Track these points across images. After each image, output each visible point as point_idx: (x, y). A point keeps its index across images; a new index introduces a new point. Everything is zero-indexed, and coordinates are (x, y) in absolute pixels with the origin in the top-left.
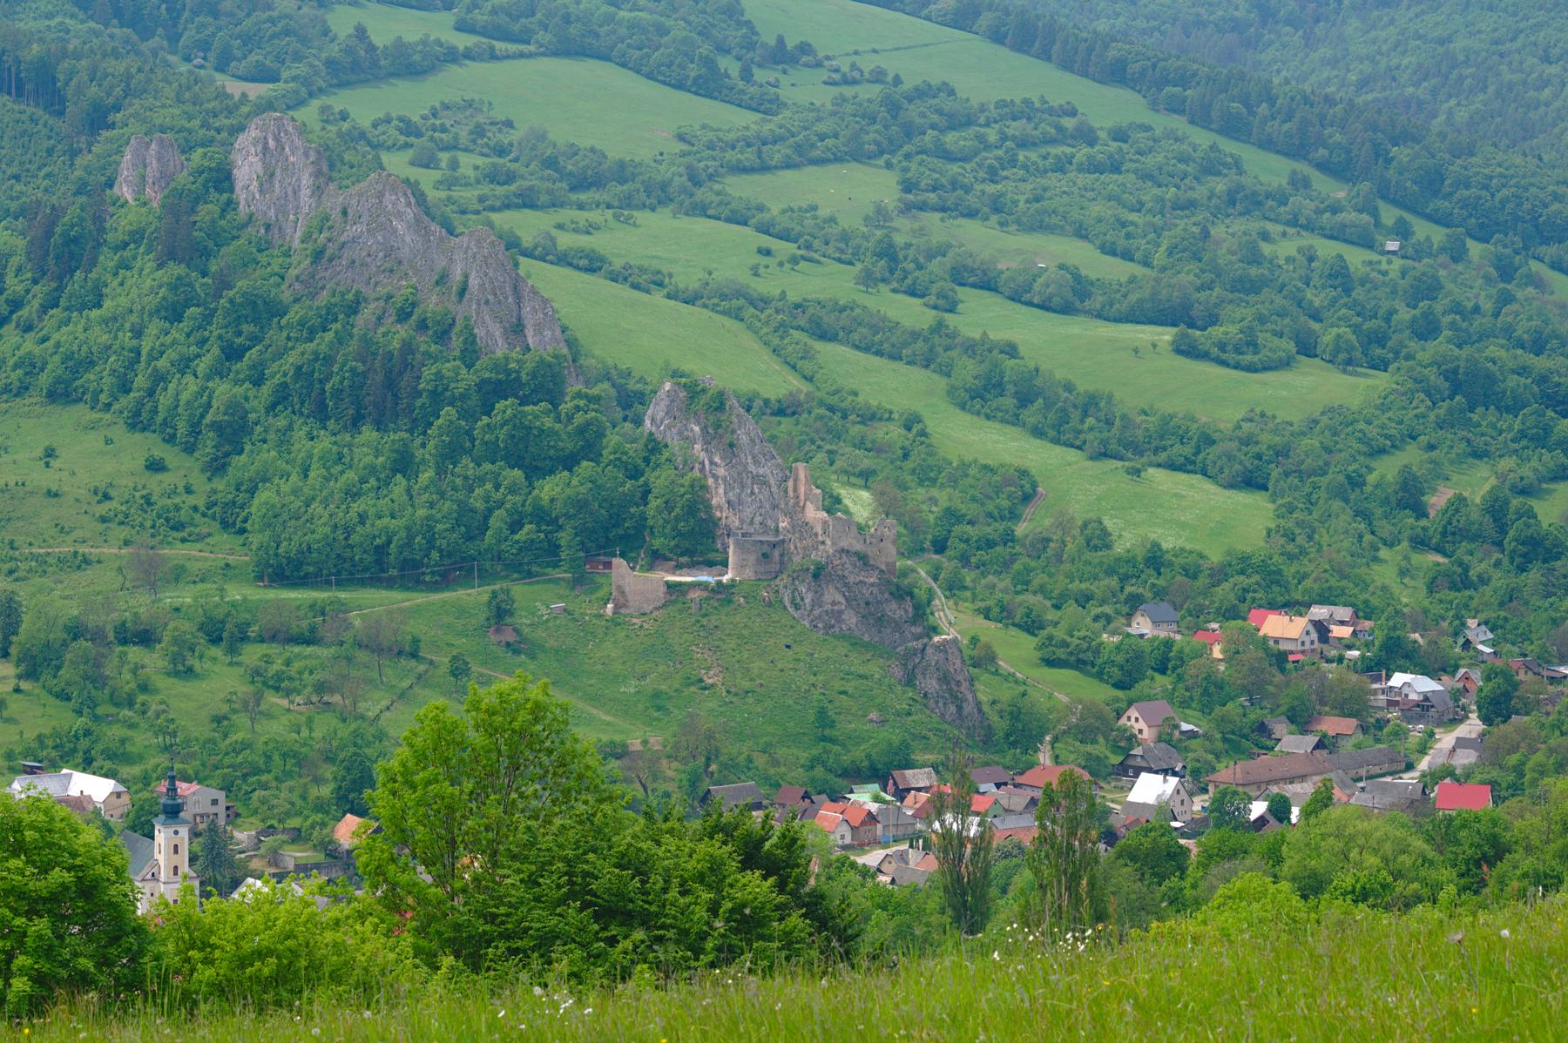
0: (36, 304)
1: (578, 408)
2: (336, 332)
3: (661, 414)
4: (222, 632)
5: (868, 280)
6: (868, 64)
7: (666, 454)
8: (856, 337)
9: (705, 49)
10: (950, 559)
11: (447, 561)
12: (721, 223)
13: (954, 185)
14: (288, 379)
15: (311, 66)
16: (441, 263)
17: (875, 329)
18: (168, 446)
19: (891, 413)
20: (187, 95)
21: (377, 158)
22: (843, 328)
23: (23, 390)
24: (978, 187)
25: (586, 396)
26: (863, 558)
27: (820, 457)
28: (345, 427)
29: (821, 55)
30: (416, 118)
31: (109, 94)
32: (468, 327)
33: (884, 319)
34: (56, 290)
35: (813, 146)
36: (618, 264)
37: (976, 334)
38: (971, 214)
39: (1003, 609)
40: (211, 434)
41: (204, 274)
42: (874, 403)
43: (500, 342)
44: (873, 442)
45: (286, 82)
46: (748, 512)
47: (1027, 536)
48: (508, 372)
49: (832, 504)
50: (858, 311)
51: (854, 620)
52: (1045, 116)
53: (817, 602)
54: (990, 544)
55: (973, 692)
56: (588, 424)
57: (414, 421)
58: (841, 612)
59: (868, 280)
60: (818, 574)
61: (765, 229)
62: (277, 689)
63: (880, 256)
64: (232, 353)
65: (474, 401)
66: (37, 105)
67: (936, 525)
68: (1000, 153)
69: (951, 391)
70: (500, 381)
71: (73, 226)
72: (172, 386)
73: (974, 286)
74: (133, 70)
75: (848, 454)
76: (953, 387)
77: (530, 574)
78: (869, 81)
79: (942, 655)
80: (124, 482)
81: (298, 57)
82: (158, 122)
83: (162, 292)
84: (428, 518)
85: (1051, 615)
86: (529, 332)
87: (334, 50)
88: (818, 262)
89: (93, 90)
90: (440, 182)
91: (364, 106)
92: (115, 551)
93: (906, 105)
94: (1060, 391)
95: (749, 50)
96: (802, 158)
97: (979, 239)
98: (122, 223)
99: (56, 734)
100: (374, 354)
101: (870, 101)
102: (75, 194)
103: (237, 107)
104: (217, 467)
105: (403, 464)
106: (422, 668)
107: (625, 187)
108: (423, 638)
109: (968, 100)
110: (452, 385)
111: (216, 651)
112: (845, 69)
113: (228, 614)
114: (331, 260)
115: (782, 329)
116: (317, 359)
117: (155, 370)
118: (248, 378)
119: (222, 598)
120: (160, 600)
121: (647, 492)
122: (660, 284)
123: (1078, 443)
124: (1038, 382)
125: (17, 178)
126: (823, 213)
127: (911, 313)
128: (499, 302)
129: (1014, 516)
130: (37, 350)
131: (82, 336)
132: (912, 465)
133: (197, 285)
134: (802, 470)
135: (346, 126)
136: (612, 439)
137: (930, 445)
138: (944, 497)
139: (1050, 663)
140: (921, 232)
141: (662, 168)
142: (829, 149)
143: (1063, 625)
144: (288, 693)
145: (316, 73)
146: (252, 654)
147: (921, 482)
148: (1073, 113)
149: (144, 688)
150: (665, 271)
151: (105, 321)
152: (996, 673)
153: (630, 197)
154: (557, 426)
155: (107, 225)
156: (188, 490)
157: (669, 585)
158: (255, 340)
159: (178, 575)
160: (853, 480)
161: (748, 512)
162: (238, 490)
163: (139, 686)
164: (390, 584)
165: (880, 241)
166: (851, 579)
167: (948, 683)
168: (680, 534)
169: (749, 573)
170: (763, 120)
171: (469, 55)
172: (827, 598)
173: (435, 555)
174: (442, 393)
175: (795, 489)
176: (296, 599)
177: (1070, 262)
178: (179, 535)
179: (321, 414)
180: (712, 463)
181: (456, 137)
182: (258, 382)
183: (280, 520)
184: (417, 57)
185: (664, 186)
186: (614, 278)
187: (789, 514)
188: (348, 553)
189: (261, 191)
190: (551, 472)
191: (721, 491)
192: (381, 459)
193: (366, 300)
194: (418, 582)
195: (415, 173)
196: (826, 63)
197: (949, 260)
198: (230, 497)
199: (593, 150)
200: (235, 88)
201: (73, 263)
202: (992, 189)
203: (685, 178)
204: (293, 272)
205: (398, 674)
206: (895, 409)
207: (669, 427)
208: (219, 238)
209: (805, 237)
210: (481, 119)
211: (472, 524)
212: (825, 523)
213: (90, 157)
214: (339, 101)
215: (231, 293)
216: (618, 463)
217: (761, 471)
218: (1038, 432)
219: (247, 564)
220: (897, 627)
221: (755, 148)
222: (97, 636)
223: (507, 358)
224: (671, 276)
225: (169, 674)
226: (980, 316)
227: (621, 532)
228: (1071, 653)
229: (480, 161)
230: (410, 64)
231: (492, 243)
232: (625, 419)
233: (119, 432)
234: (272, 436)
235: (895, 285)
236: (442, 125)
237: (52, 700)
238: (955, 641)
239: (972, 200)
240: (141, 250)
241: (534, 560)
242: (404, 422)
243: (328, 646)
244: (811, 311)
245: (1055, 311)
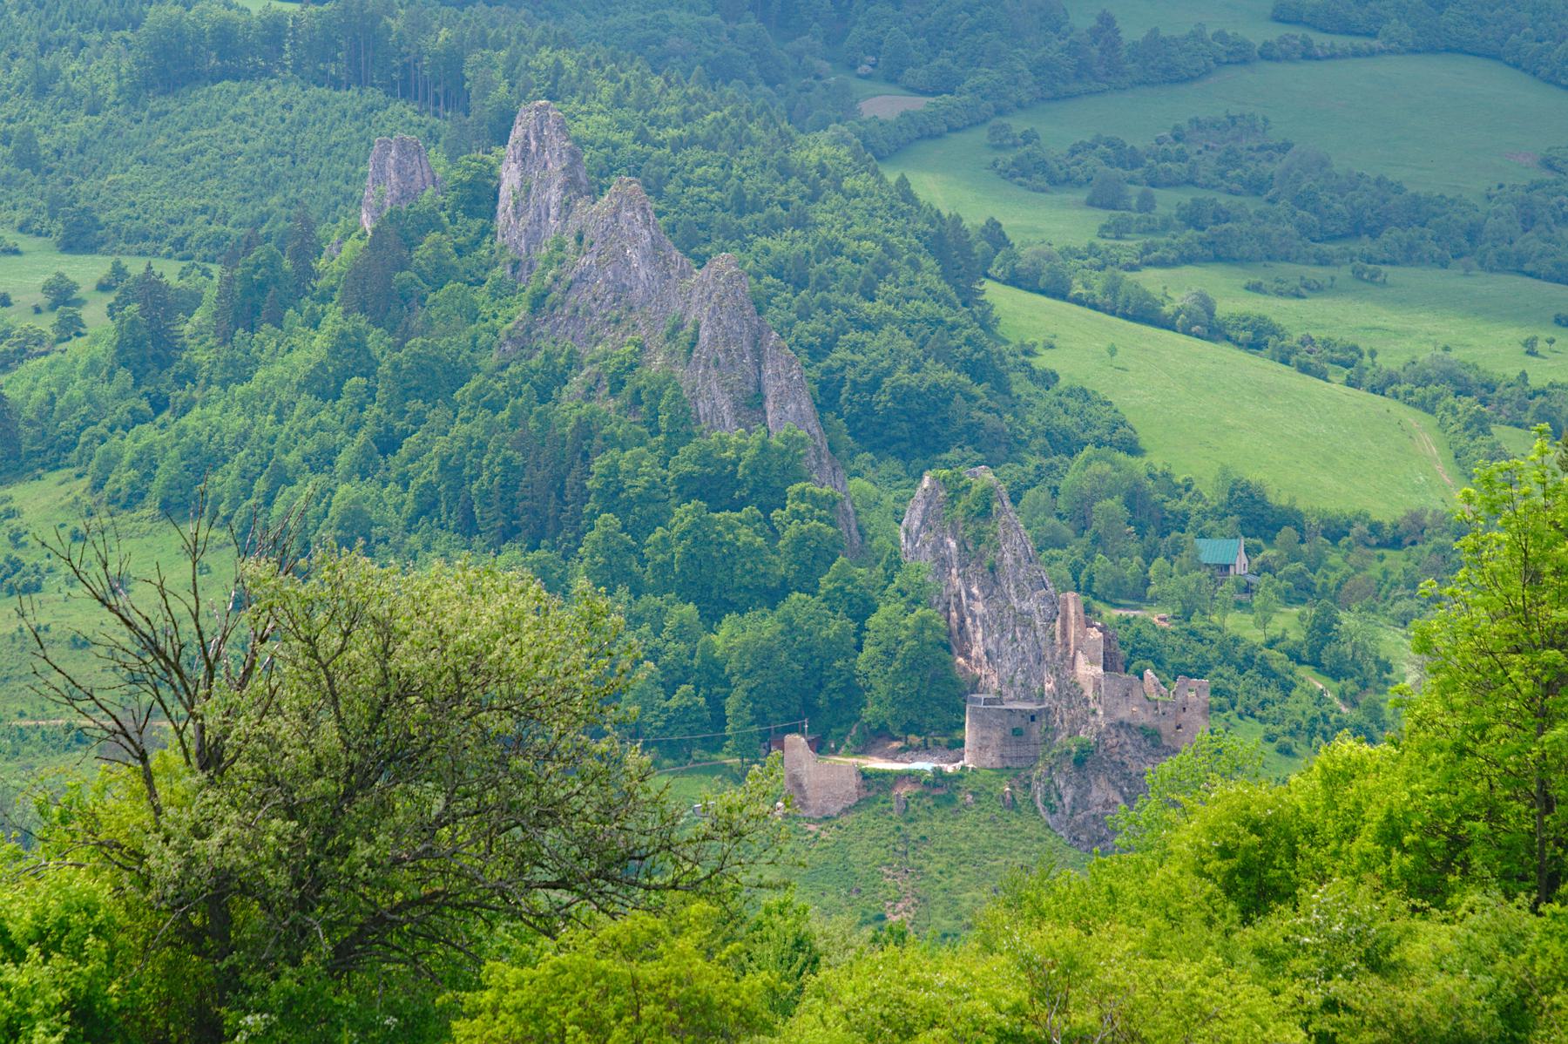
36: (1293, 341)
53: (1080, 802)
71: (258, 266)
90: (1106, 227)
110: (629, 482)
153: (1411, 248)
157: (865, 776)
169: (991, 758)
171: (1267, 54)
172: (1097, 795)
187: (1057, 672)
191: (979, 636)
217: (1025, 606)
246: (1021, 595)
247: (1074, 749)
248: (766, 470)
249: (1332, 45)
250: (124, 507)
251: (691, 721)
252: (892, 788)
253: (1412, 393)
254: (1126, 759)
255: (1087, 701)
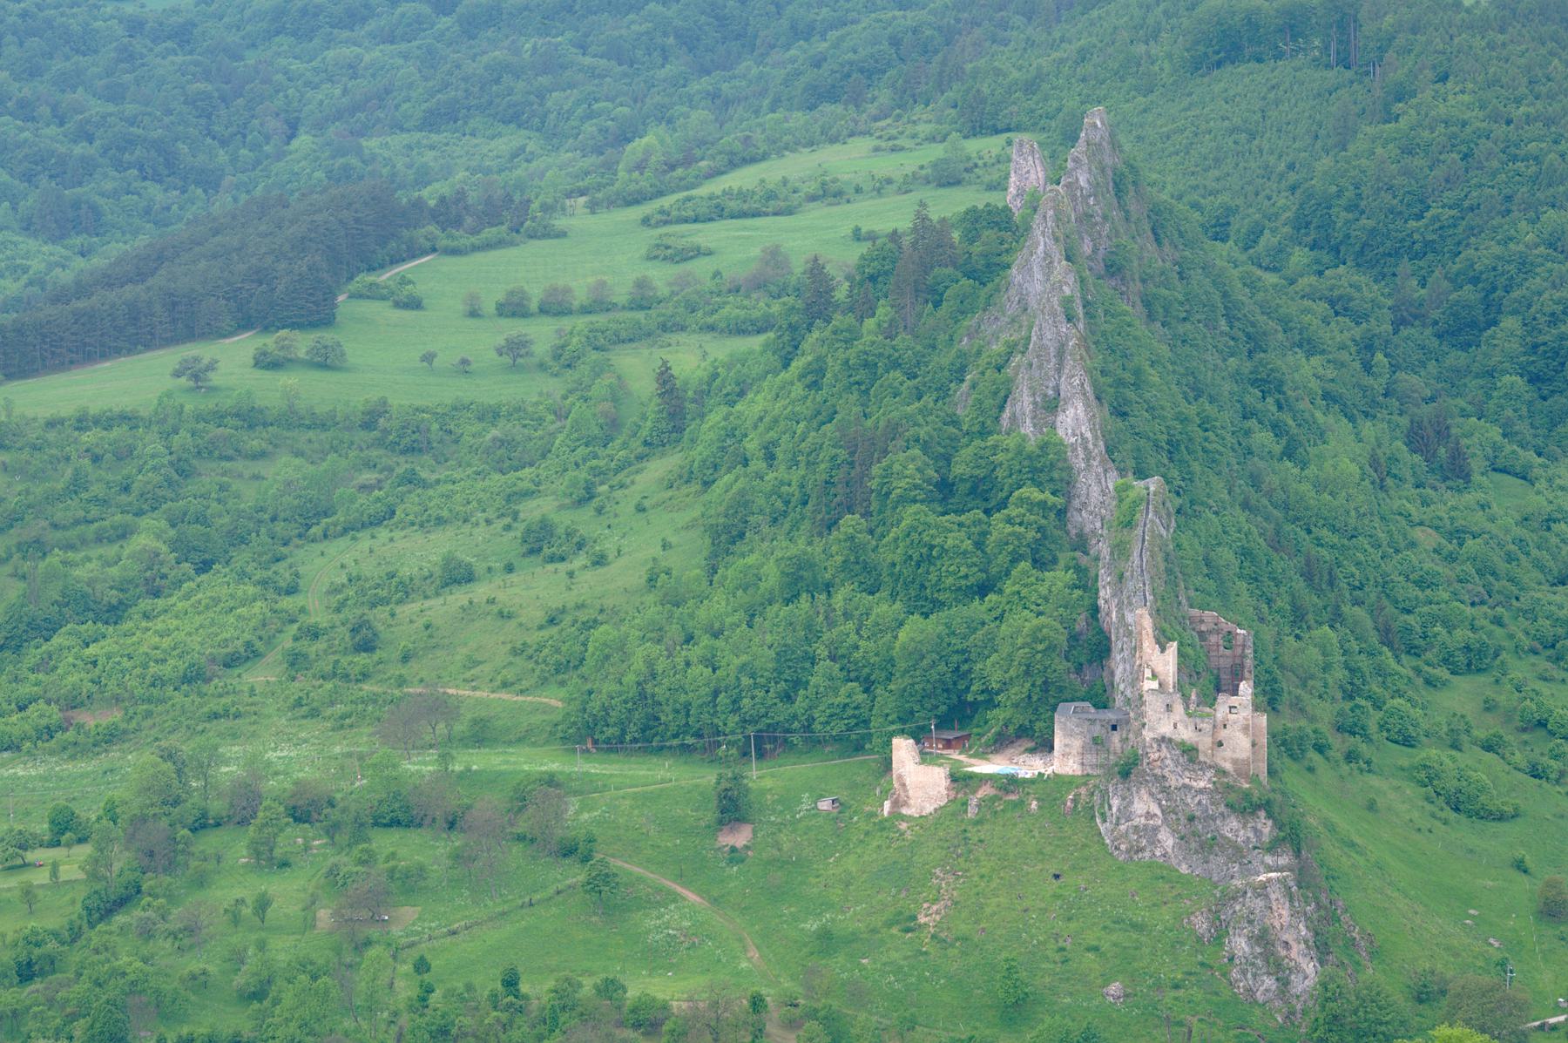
51: (1170, 842)
58: (1156, 829)
166: (1173, 782)
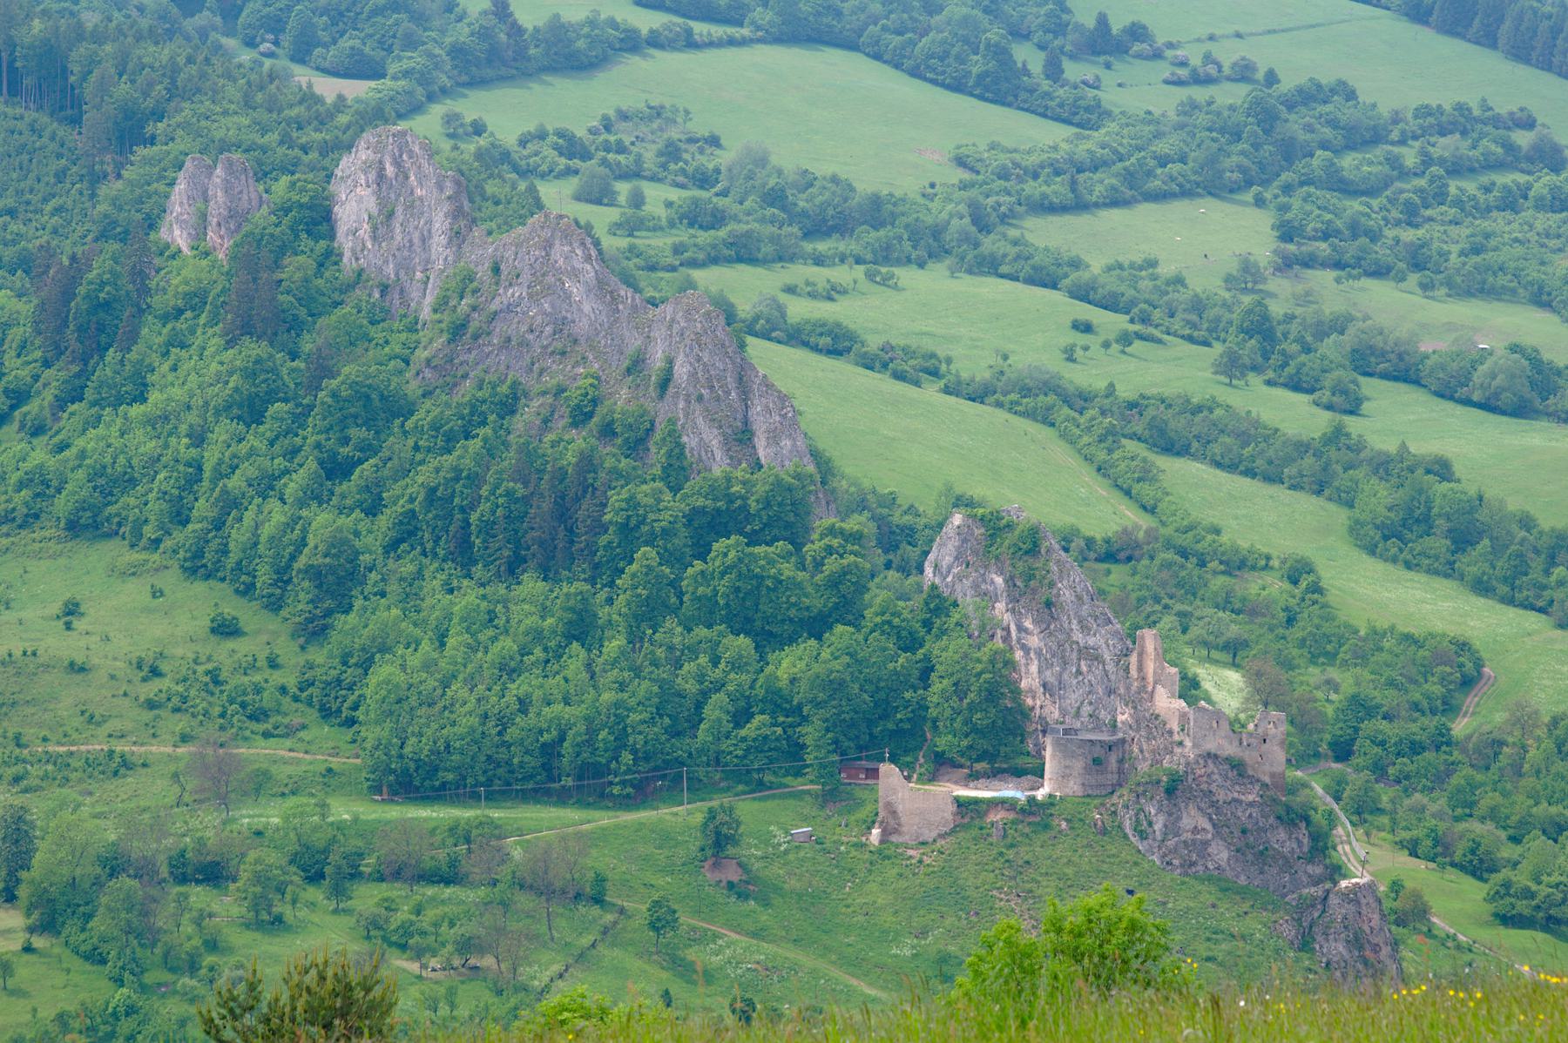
0: (49, 396)
1: (830, 550)
2: (485, 440)
3: (948, 559)
4: (323, 866)
5: (1232, 368)
6: (1228, 54)
7: (956, 617)
8: (1216, 449)
9: (994, 34)
10: (1358, 770)
11: (643, 766)
12: (1019, 286)
13: (1355, 230)
14: (416, 506)
15: (430, 55)
16: (634, 342)
17: (1244, 438)
18: (243, 601)
19: (1268, 558)
20: (259, 97)
21: (532, 190)
22: (1197, 437)
23: (31, 518)
24: (1390, 233)
25: (842, 532)
26: (1237, 767)
27: (1168, 621)
28: (498, 575)
29: (1160, 41)
30: (581, 133)
31: (146, 94)
32: (674, 435)
33: (1257, 424)
34: (78, 375)
35: (1150, 174)
36: (873, 343)
37: (1390, 446)
38: (1380, 272)
39: (1437, 842)
40: (306, 584)
41: (294, 356)
42: (1244, 544)
43: (718, 455)
44: (1244, 600)
45: (394, 78)
46: (1073, 698)
47: (1469, 737)
48: (730, 499)
49: (1189, 688)
50: (1218, 412)
51: (1225, 855)
52: (1489, 129)
53: (1172, 829)
54: (1416, 748)
55: (1398, 961)
56: (845, 572)
57: (596, 566)
58: (1206, 843)
59: (1232, 368)
60: (1174, 789)
61: (1083, 294)
62: (403, 947)
63: (1249, 333)
64: (336, 469)
65: (681, 539)
66: (40, 108)
67: (1337, 720)
68: (1422, 182)
69: (1355, 529)
70: (718, 511)
72: (249, 516)
73: (1385, 376)
74: (181, 60)
75: (1210, 619)
76: (1357, 522)
77: (761, 785)
78: (1229, 79)
79: (1352, 908)
80: (179, 652)
81: (411, 43)
82: (219, 134)
83: (234, 381)
84: (617, 705)
85: (1508, 852)
86: (761, 443)
87: (461, 33)
88: (1160, 341)
89: (123, 89)
90: (618, 225)
91: (508, 114)
92: (169, 750)
93: (1285, 115)
94: (1515, 528)
95: (1056, 34)
96: (1136, 189)
97: (1392, 308)
98: (174, 282)
99: (86, 1010)
100: (539, 471)
101: (1232, 108)
102: (96, 240)
103: (332, 116)
104: (314, 631)
105: (581, 628)
106: (609, 918)
107: (882, 233)
108: (609, 875)
109: (1374, 106)
110: (651, 516)
111: (315, 894)
112: (1196, 61)
113: (334, 840)
114: (476, 337)
115: (1110, 437)
116: (457, 479)
117: (225, 491)
118: (358, 504)
119: (324, 816)
120: (234, 820)
121: (927, 671)
122: (934, 373)
123: (1540, 604)
124: (1482, 515)
125: (11, 213)
126: (1166, 270)
127: (1295, 416)
128: (718, 399)
129: (1449, 707)
130: (52, 462)
131: (117, 443)
132: (1300, 635)
133: (285, 371)
134: (1149, 639)
135: (482, 142)
136: (877, 596)
137: (1325, 606)
138: (1347, 680)
139: (1508, 920)
140: (1306, 298)
141: (935, 205)
142: (1172, 179)
143: (1526, 866)
144: (419, 954)
145: (437, 66)
146: (367, 897)
147: (1313, 660)
148: (1529, 124)
149: (212, 945)
150: (941, 354)
151: (151, 422)
152: (1430, 933)
153: (888, 248)
154: (801, 575)
155: (153, 285)
156: (273, 664)
157: (962, 805)
158: (368, 450)
159: (260, 785)
160: (1215, 654)
161: (1073, 698)
162: (345, 663)
163: (206, 943)
164: (562, 798)
165: (1249, 312)
166: (1221, 796)
167: (1361, 948)
168: (975, 730)
169: (1074, 787)
170: (1077, 136)
171: (656, 41)
172: (1187, 822)
173: (626, 757)
174: (637, 527)
175: (1140, 668)
176: (426, 820)
177: (1528, 341)
178: (261, 727)
179: (463, 556)
180: (1020, 628)
181: (639, 160)
182: (372, 510)
183: (406, 706)
184: (581, 44)
185: (937, 232)
186: (868, 363)
188: (502, 755)
189: (374, 238)
190: (792, 640)
191: (1034, 668)
192: (550, 621)
193: (526, 395)
194: (602, 796)
195: (585, 212)
196: (1169, 53)
197: (1348, 339)
198: (334, 673)
199: (835, 179)
200: (328, 88)
201: (103, 339)
202: (1409, 235)
203: (967, 220)
204: (422, 354)
205: (576, 926)
206: (1275, 554)
207: (960, 578)
208: (314, 304)
209: (1143, 306)
210: (674, 134)
211: (681, 715)
212: (1183, 717)
213: (119, 184)
214: (470, 106)
215: (334, 383)
216: (887, 628)
217: (1091, 641)
218: (1482, 588)
219: (358, 769)
220: (1287, 865)
221: (1067, 177)
222: (144, 871)
223: (728, 479)
224: (949, 361)
225: (247, 926)
226: (1396, 420)
227: (891, 726)
228: (1538, 907)
229: (675, 195)
230: (573, 53)
231: (708, 313)
232: (888, 566)
233: (171, 579)
234: (393, 588)
235: (1271, 374)
236: (619, 142)
237: (77, 963)
238: (1371, 887)
239: (1381, 252)
240: (203, 320)
241: (768, 765)
242: (582, 567)
243: (473, 885)
244: (1150, 412)
245: (1504, 413)
246: (1085, 629)
247: (1165, 779)
248: (780, 505)
249: (709, 34)
250: (20, 527)
251: (770, 750)
252: (986, 813)
253: (1018, 403)
254: (1214, 788)
255: (1171, 732)
